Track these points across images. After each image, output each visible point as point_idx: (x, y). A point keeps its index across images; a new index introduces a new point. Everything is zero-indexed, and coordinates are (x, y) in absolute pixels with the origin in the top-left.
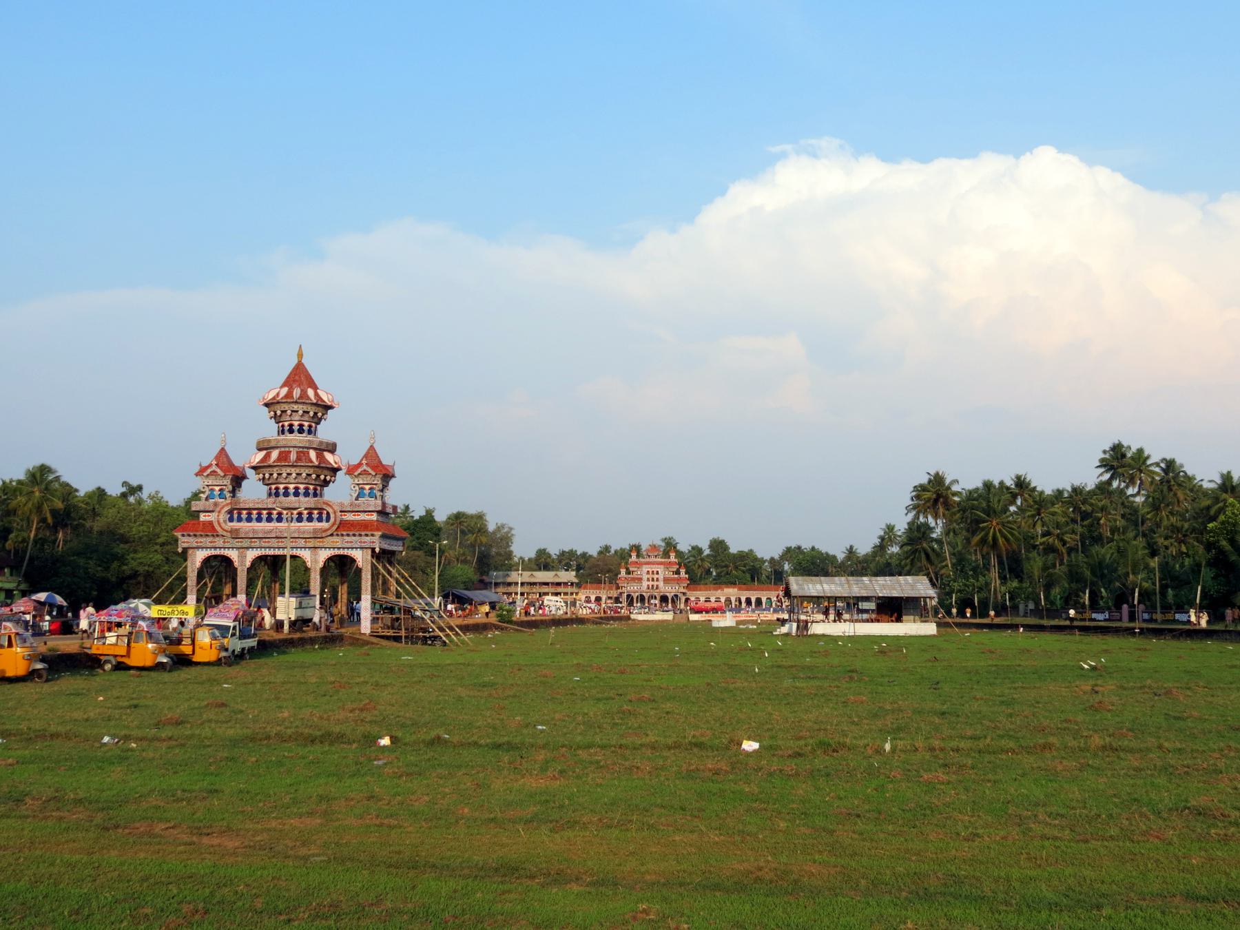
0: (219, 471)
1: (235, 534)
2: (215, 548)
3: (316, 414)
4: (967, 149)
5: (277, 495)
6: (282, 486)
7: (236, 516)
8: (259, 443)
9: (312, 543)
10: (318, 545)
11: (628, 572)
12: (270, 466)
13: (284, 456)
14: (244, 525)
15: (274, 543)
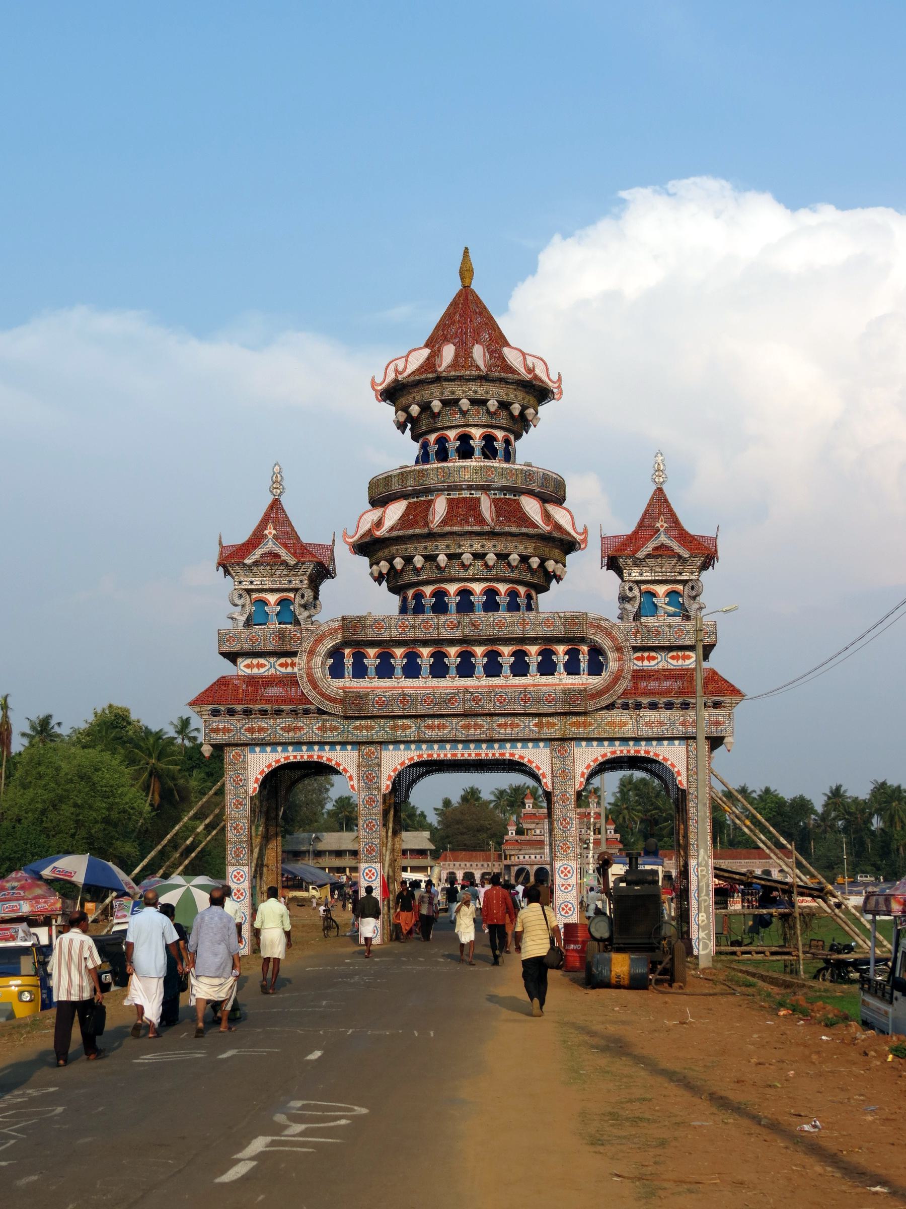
0: (282, 552)
1: (355, 709)
2: (298, 744)
3: (504, 405)
4: (687, 176)
5: (440, 607)
6: (452, 588)
7: (348, 661)
8: (373, 485)
9: (556, 727)
10: (574, 731)
11: (520, 832)
12: (431, 536)
13: (463, 509)
14: (372, 684)
15: (453, 728)
